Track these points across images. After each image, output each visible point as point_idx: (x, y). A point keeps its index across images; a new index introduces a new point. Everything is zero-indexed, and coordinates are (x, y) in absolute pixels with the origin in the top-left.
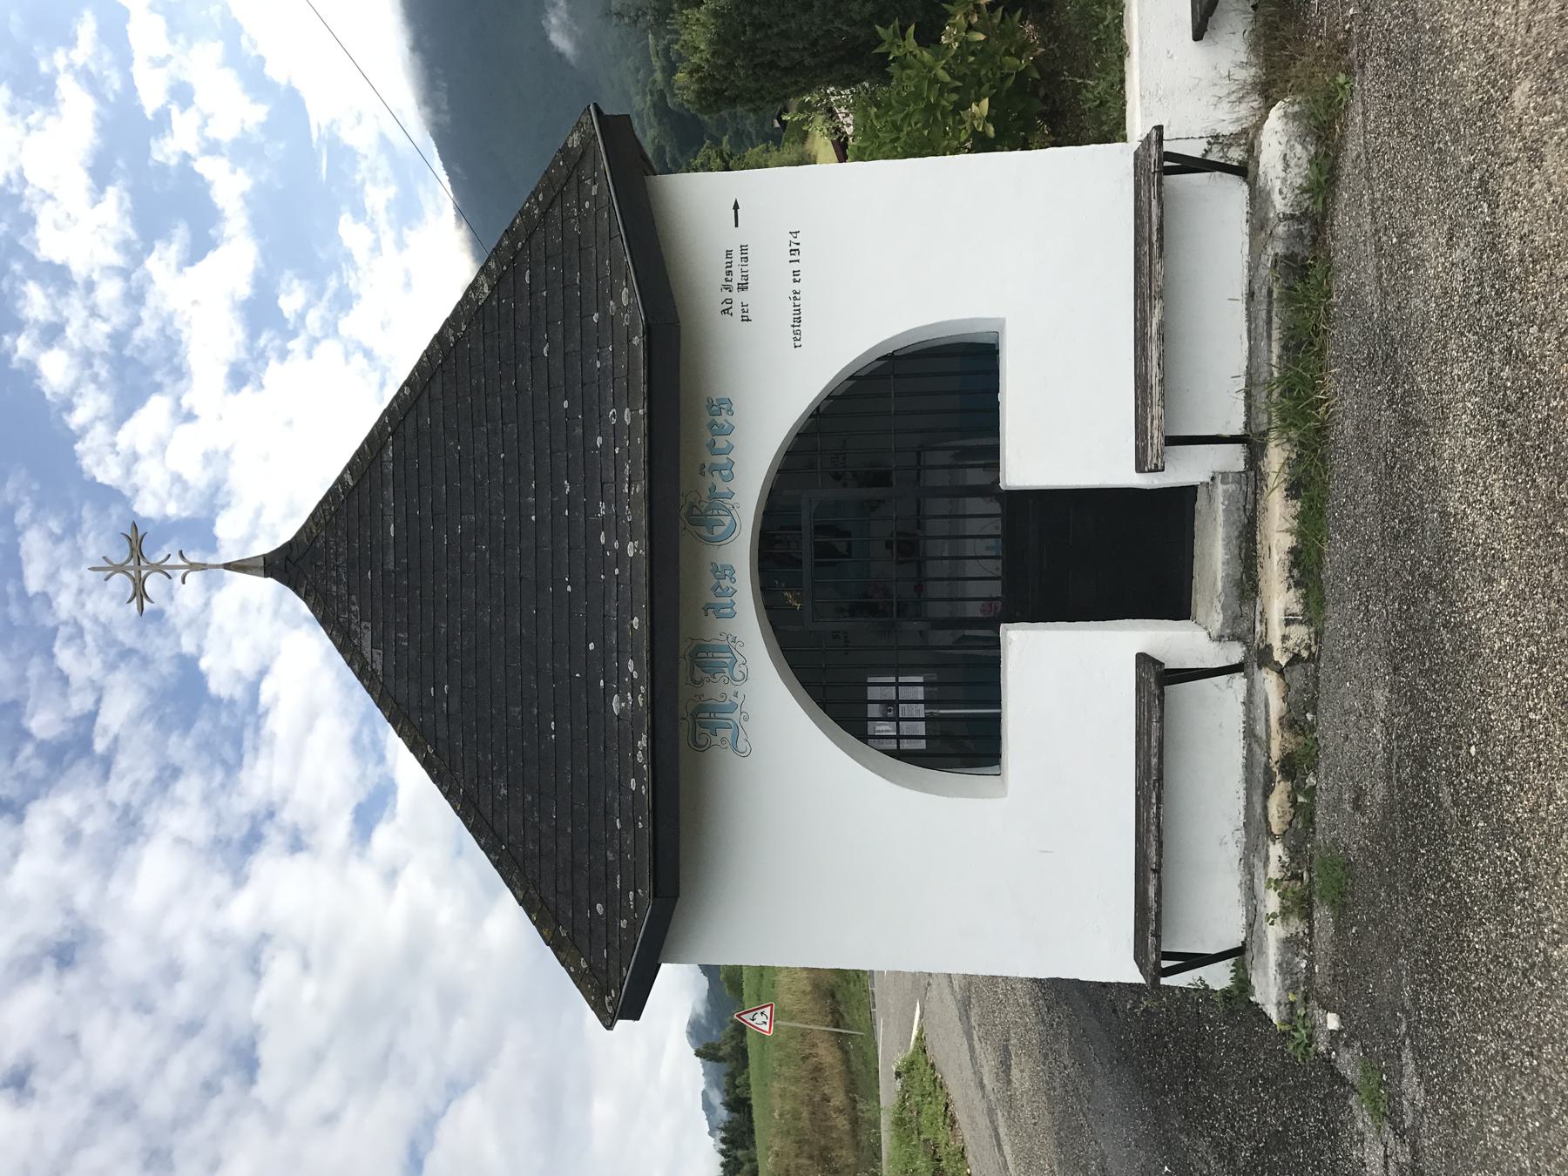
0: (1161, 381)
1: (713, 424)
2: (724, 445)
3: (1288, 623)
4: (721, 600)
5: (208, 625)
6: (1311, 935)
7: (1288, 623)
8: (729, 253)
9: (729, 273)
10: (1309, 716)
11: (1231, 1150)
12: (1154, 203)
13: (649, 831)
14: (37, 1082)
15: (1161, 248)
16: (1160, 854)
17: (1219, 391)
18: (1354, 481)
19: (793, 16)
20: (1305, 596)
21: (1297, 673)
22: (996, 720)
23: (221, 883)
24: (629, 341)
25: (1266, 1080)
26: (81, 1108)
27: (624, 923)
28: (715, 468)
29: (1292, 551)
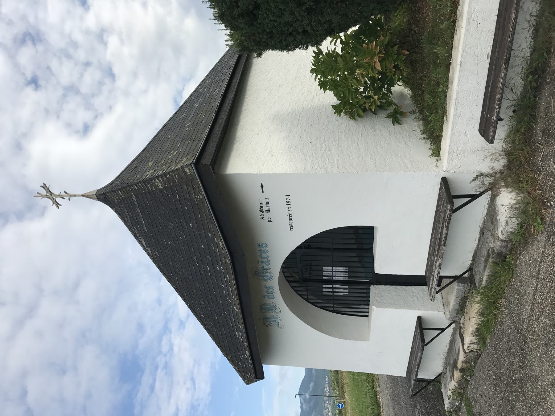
1: (260, 251)
8: (260, 201)
9: (261, 207)
12: (445, 229)
14: (41, 82)
15: (445, 243)
23: (79, 10)
26: (60, 92)
28: (262, 262)
29: (477, 328)
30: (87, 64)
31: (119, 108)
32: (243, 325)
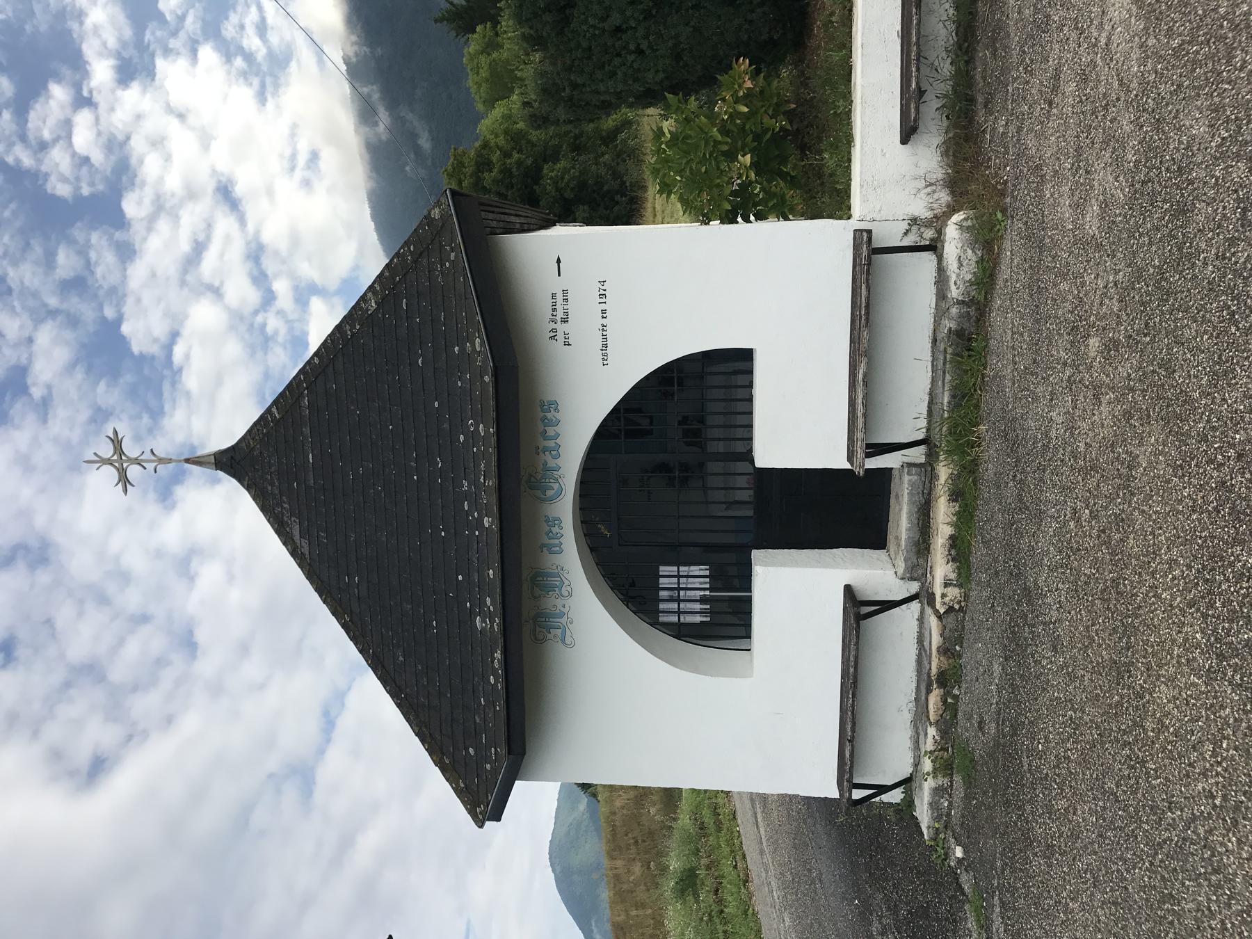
0: (864, 415)
2: (553, 434)
3: (946, 585)
4: (552, 541)
5: (125, 295)
6: (952, 786)
7: (946, 585)
8: (554, 295)
10: (958, 648)
11: (895, 906)
12: (864, 287)
13: (503, 715)
14: (21, 652)
16: (853, 730)
17: (910, 405)
18: (989, 510)
19: (602, 81)
20: (958, 568)
21: (951, 619)
22: (749, 600)
24: (482, 377)
25: (919, 872)
27: (488, 767)
28: (545, 450)
29: (951, 537)
30: (143, 619)
31: (190, 723)
32: (498, 571)
